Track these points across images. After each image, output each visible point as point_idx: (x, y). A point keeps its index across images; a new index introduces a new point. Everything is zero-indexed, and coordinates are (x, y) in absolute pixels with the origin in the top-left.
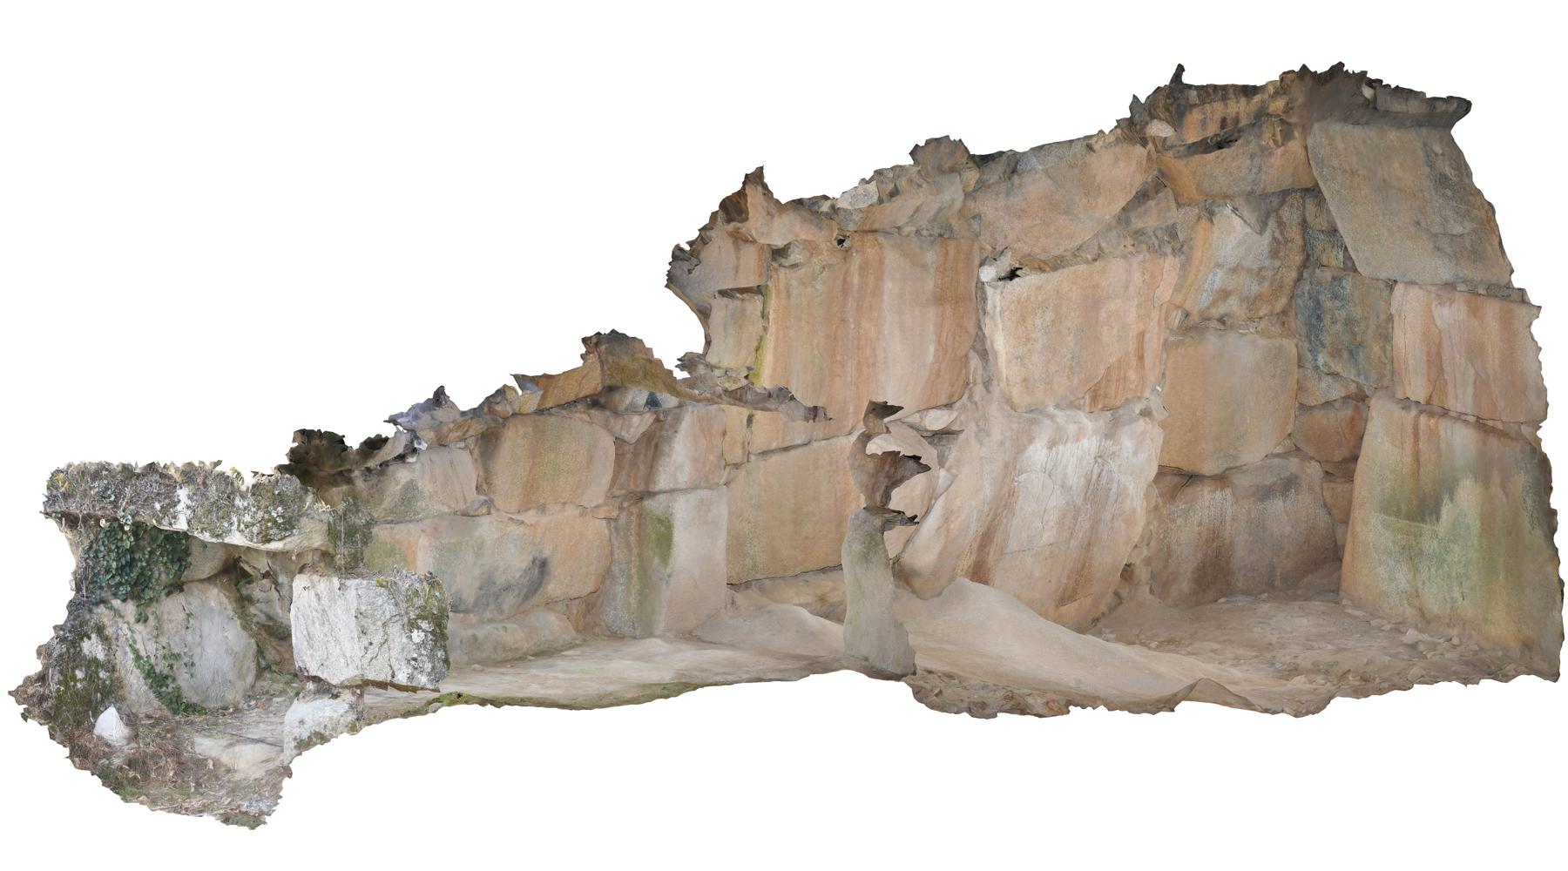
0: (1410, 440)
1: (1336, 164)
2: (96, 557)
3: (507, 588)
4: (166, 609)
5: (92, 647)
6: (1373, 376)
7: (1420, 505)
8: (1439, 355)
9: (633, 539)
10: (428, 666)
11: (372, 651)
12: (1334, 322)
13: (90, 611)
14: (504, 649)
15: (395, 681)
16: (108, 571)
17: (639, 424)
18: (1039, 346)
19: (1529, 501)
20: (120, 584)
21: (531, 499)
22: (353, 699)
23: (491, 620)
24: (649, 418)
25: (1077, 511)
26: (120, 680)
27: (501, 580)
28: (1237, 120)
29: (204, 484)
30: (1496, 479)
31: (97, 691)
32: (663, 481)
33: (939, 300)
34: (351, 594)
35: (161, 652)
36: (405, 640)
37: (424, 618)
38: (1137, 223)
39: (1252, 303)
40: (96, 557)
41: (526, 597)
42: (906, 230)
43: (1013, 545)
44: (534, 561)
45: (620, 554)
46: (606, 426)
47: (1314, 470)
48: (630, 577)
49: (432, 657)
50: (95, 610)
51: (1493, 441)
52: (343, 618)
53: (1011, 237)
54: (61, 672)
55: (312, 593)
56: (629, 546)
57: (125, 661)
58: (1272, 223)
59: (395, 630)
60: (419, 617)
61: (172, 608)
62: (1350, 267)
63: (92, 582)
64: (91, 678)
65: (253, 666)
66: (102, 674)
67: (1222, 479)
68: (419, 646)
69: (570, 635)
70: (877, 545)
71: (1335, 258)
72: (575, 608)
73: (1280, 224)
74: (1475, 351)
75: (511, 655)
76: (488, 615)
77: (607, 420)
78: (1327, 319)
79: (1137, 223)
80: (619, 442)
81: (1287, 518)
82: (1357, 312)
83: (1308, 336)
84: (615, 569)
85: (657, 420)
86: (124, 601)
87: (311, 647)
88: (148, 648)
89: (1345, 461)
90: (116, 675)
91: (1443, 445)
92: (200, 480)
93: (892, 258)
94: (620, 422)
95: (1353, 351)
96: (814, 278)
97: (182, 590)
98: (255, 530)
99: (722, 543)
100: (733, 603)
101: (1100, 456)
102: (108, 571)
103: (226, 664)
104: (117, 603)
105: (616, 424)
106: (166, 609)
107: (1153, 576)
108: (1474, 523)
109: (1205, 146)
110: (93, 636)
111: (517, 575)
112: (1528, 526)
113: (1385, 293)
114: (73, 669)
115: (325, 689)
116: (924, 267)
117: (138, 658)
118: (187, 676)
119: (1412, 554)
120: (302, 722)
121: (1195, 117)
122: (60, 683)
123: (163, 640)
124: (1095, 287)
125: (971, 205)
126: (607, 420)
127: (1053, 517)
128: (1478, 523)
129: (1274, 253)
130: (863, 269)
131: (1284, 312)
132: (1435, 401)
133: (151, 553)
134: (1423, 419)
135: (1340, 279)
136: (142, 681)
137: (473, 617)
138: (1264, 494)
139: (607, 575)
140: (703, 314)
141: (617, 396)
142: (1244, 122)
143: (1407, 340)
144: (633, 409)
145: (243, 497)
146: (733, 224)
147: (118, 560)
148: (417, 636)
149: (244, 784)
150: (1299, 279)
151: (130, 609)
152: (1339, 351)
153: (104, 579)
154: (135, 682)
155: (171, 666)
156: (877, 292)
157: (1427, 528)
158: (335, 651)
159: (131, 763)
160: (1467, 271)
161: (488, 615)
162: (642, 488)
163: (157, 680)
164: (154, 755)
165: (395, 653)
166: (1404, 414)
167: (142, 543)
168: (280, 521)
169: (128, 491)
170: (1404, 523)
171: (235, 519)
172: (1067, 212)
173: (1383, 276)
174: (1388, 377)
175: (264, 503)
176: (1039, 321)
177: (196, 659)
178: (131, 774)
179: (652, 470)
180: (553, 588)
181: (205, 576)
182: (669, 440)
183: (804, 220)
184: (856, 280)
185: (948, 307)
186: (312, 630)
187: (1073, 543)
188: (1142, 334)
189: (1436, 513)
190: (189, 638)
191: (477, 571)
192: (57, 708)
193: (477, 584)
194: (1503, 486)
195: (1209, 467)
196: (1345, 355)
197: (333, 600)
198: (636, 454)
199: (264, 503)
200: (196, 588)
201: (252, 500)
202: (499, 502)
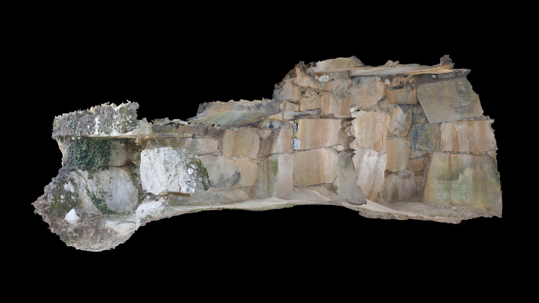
0: (448, 161)
1: (425, 95)
2: (72, 153)
3: (228, 180)
4: (102, 175)
6: (433, 148)
7: (452, 176)
8: (457, 138)
9: (265, 169)
10: (195, 184)
11: (172, 178)
12: (421, 136)
13: (68, 173)
14: (227, 199)
15: (181, 191)
16: (76, 159)
17: (267, 133)
19: (490, 171)
20: (81, 163)
21: (234, 153)
22: (164, 201)
23: (223, 190)
24: (270, 131)
26: (80, 200)
27: (226, 177)
29: (103, 113)
30: (478, 167)
31: (69, 204)
32: (274, 151)
34: (162, 153)
35: (98, 191)
36: (185, 173)
37: (193, 163)
38: (382, 106)
39: (401, 132)
40: (72, 153)
41: (234, 184)
42: (335, 92)
44: (236, 172)
45: (261, 175)
46: (257, 133)
47: (413, 174)
48: (264, 181)
49: (197, 181)
50: (70, 173)
51: (477, 157)
52: (160, 167)
53: (358, 101)
54: (54, 195)
55: (147, 157)
56: (264, 172)
57: (83, 193)
58: (407, 112)
59: (181, 169)
60: (191, 163)
61: (104, 175)
62: (427, 121)
63: (71, 163)
64: (67, 199)
65: (137, 198)
66: (73, 198)
68: (191, 175)
69: (247, 197)
70: (350, 162)
71: (422, 120)
72: (248, 190)
73: (408, 113)
74: (470, 135)
75: (229, 201)
76: (222, 189)
77: (257, 131)
78: (419, 136)
79: (382, 106)
80: (261, 139)
81: (409, 183)
82: (429, 132)
83: (413, 141)
84: (260, 179)
85: (272, 132)
86: (83, 170)
87: (147, 180)
88: (93, 189)
89: (421, 171)
90: (79, 198)
91: (459, 160)
92: (101, 112)
93: (331, 99)
94: (261, 131)
95: (427, 142)
96: (312, 101)
97: (108, 169)
98: (121, 127)
99: (291, 171)
100: (294, 190)
102: (76, 159)
103: (126, 197)
104: (80, 171)
105: (260, 132)
106: (102, 175)
107: (383, 196)
108: (470, 179)
109: (396, 88)
110: (69, 183)
111: (231, 176)
112: (489, 177)
113: (438, 126)
114: (59, 195)
115: (154, 198)
117: (88, 192)
118: (109, 200)
119: (448, 189)
120: (143, 211)
122: (53, 200)
123: (100, 187)
124: (375, 118)
125: (349, 90)
126: (257, 131)
127: (367, 176)
129: (406, 121)
130: (325, 100)
131: (406, 136)
132: (455, 150)
133: (94, 152)
134: (452, 155)
136: (90, 201)
137: (217, 189)
138: (405, 178)
139: (257, 181)
141: (260, 124)
142: (405, 84)
143: (446, 135)
144: (265, 128)
145: (116, 114)
146: (292, 79)
147: (81, 154)
148: (190, 171)
149: (120, 238)
150: (411, 127)
151: (86, 174)
153: (75, 162)
154: (87, 202)
155: (103, 196)
157: (454, 182)
158: (156, 180)
159: (76, 230)
160: (466, 115)
161: (222, 189)
162: (268, 153)
163: (97, 201)
164: (86, 228)
165: (180, 179)
166: (446, 154)
167: (91, 149)
168: (130, 122)
169: (79, 123)
170: (446, 182)
171: (113, 124)
172: (371, 95)
173: (438, 122)
174: (439, 147)
175: (124, 115)
177: (114, 195)
178: (74, 235)
179: (271, 147)
180: (242, 183)
181: (118, 165)
182: (276, 138)
183: (312, 80)
184: (323, 104)
186: (148, 173)
187: (370, 184)
188: (383, 134)
189: (457, 178)
190: (111, 187)
191: (218, 174)
192: (51, 210)
193: (218, 178)
194: (481, 168)
195: (394, 170)
196: (424, 144)
197: (155, 159)
198: (266, 144)
199: (124, 115)
200: (115, 169)
201: (119, 115)
202: (225, 153)
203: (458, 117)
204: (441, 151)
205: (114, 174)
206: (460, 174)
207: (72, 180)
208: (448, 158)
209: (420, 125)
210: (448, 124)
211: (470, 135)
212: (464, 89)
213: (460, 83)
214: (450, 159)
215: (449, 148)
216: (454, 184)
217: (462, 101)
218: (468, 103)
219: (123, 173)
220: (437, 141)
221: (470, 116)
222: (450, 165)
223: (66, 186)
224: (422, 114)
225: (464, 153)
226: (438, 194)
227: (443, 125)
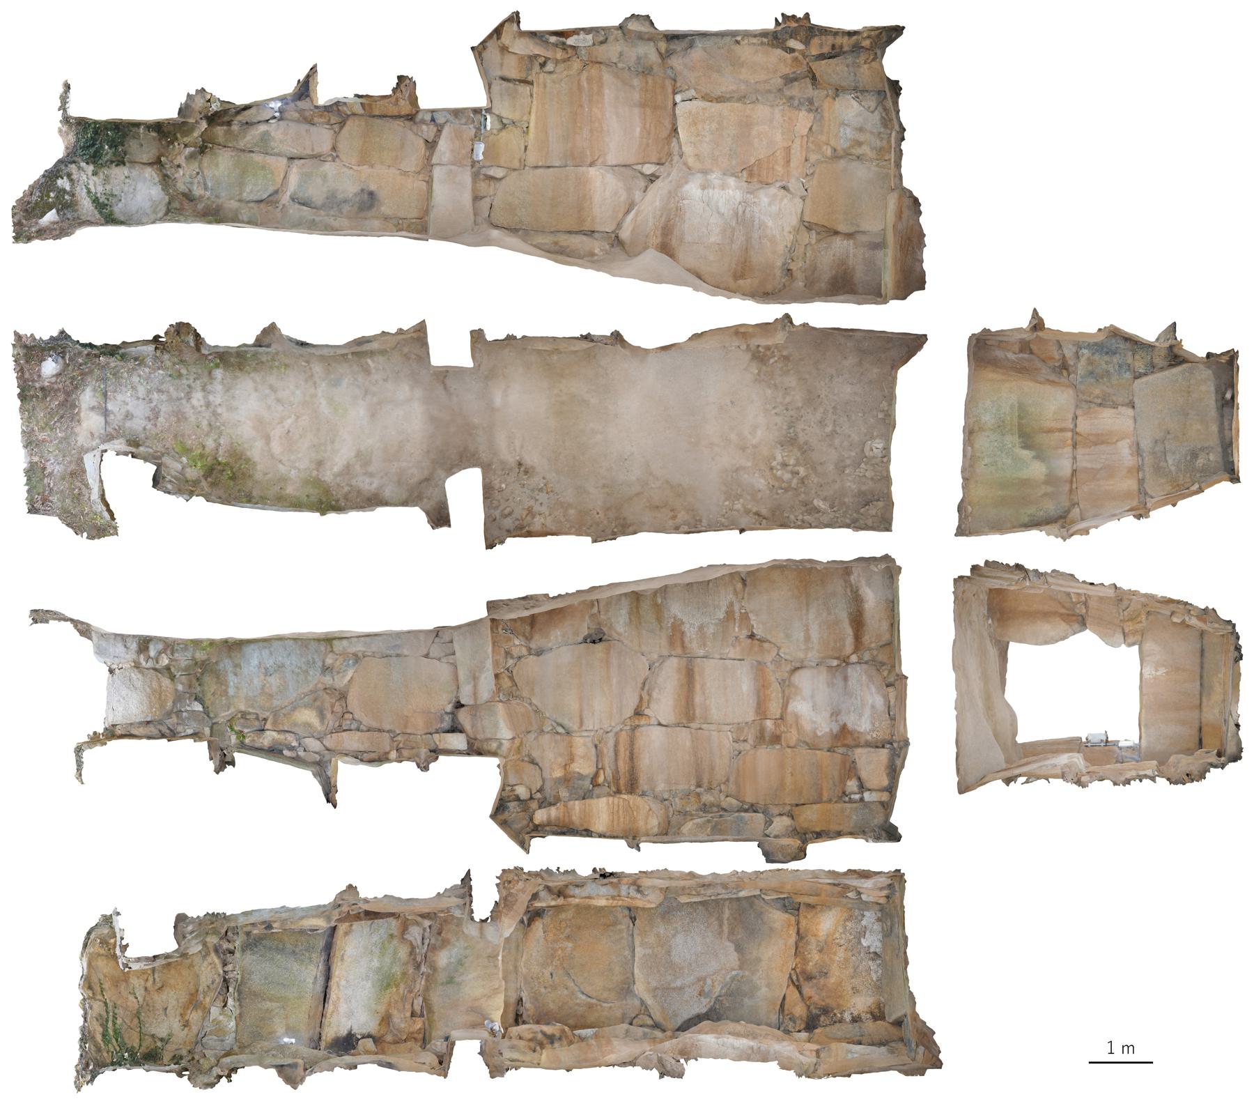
0: (1059, 426)
5: (63, 183)
8: (1103, 443)
12: (1107, 363)
18: (707, 139)
25: (733, 230)
27: (340, 196)
28: (841, 47)
33: (643, 105)
43: (688, 238)
44: (362, 190)
57: (81, 193)
61: (119, 173)
62: (1138, 376)
65: (164, 209)
66: (67, 197)
67: (849, 236)
78: (1106, 358)
82: (1114, 380)
91: (1060, 451)
93: (607, 77)
101: (744, 202)
103: (147, 205)
104: (83, 164)
109: (822, 57)
113: (1127, 401)
114: (49, 192)
116: (632, 87)
117: (89, 192)
119: (1000, 427)
121: (816, 41)
123: (108, 187)
132: (1079, 438)
134: (1069, 434)
140: (489, 87)
143: (1108, 420)
151: (91, 168)
156: (600, 93)
157: (1016, 439)
161: (332, 212)
170: (1016, 421)
172: (718, 71)
173: (1136, 400)
174: (1086, 402)
176: (707, 127)
185: (648, 111)
189: (1026, 446)
191: (325, 189)
195: (842, 228)
196: (1090, 368)
200: (137, 167)
203: (1146, 444)
204: (1077, 406)
205: (135, 173)
206: (1033, 453)
207: (69, 175)
208: (1064, 425)
209: (1130, 361)
210: (1131, 422)
211: (1110, 471)
212: (1200, 462)
213: (1212, 457)
214: (1062, 430)
215: (1084, 426)
216: (1012, 440)
217: (1178, 456)
218: (1173, 468)
219: (149, 172)
220: (1098, 397)
221: (1146, 469)
222: (1050, 431)
223: (60, 182)
225: (1074, 458)
226: (988, 403)
227: (1130, 412)
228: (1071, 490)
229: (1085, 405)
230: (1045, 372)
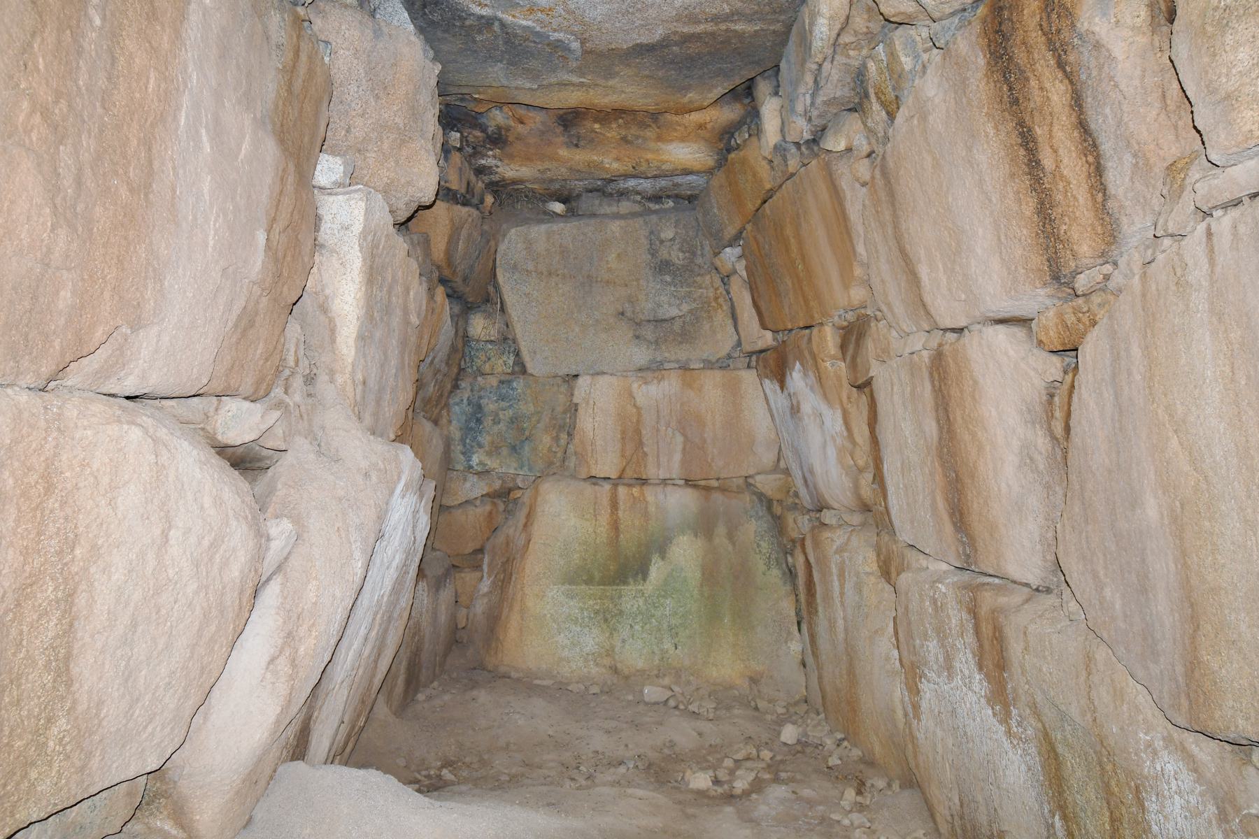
12: (496, 421)
30: (721, 530)
62: (521, 368)
71: (502, 364)
74: (688, 423)
78: (488, 422)
82: (527, 408)
112: (761, 567)
128: (698, 575)
134: (622, 490)
135: (509, 382)
152: (497, 448)
157: (630, 589)
171: (1108, 111)
173: (563, 371)
189: (643, 572)
194: (731, 536)
196: (505, 451)
209: (494, 381)
212: (677, 257)
213: (668, 234)
218: (685, 308)
224: (506, 340)
227: (583, 382)
228: (723, 490)
229: (572, 463)
230: (512, 529)
